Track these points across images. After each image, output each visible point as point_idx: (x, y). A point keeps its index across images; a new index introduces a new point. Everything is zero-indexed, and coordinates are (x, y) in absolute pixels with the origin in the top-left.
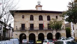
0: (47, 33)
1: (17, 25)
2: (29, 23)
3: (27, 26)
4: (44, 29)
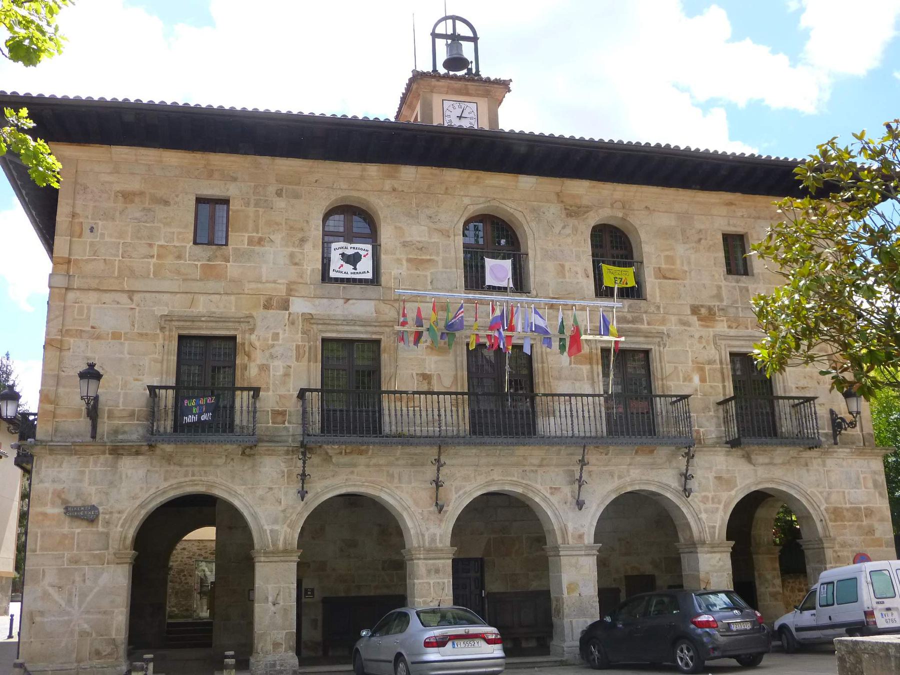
0: (601, 493)
1: (100, 354)
2: (309, 319)
3: (280, 371)
4: (548, 425)
